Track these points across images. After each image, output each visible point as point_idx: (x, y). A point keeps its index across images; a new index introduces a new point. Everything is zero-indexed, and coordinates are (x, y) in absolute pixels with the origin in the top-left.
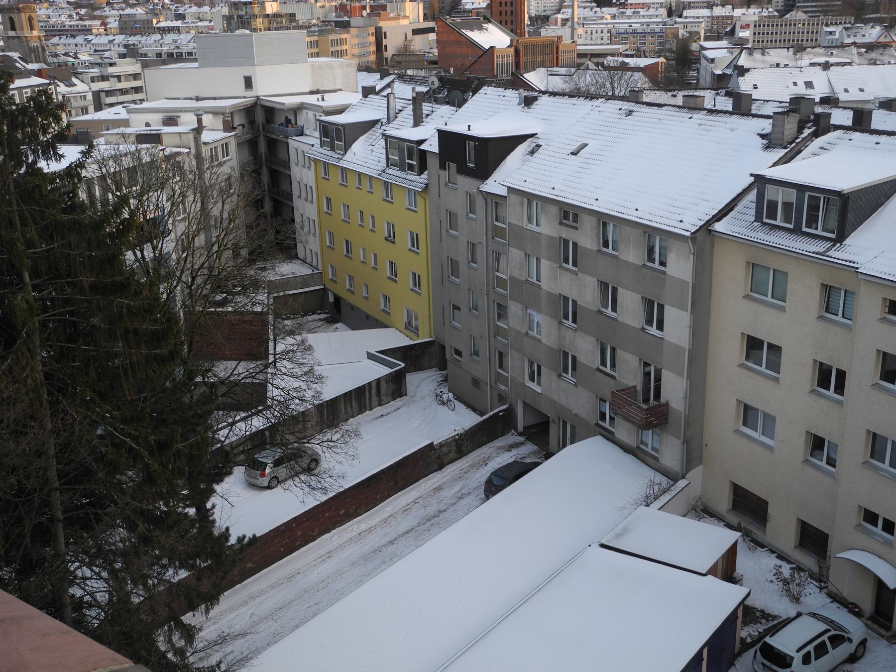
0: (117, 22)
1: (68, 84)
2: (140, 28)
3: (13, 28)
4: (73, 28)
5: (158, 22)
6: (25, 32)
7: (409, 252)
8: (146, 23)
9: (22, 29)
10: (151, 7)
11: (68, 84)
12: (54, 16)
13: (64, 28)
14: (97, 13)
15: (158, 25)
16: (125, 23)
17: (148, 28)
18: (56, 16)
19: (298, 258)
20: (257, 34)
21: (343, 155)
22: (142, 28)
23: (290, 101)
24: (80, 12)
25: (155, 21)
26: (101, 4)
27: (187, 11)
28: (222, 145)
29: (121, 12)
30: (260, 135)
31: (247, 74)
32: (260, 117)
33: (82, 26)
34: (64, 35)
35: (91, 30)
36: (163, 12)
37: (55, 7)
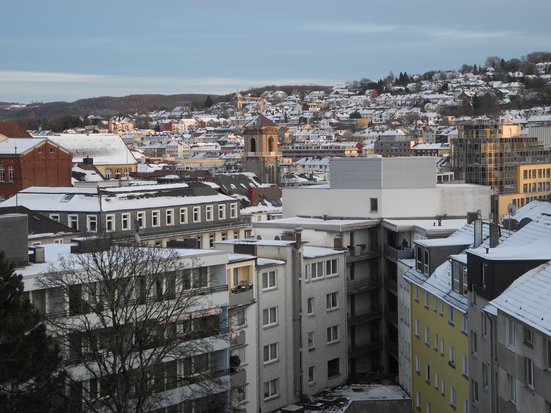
0: (373, 144)
1: (275, 203)
2: (396, 150)
3: (253, 149)
4: (326, 149)
5: (416, 144)
6: (263, 153)
7: (463, 377)
8: (403, 145)
9: (261, 150)
10: (413, 129)
11: (275, 203)
12: (314, 137)
13: (318, 150)
14: (357, 134)
15: (415, 148)
16: (382, 145)
17: (405, 150)
18: (315, 137)
19: (398, 384)
20: (386, 158)
21: (428, 277)
22: (398, 151)
23: (400, 224)
24: (340, 134)
25: (412, 143)
26: (363, 125)
27: (449, 134)
28: (328, 262)
29: (381, 134)
30: (381, 257)
31: (374, 197)
32: (382, 239)
33: (336, 147)
34: (310, 156)
35: (343, 152)
36: (425, 134)
37: (316, 128)
